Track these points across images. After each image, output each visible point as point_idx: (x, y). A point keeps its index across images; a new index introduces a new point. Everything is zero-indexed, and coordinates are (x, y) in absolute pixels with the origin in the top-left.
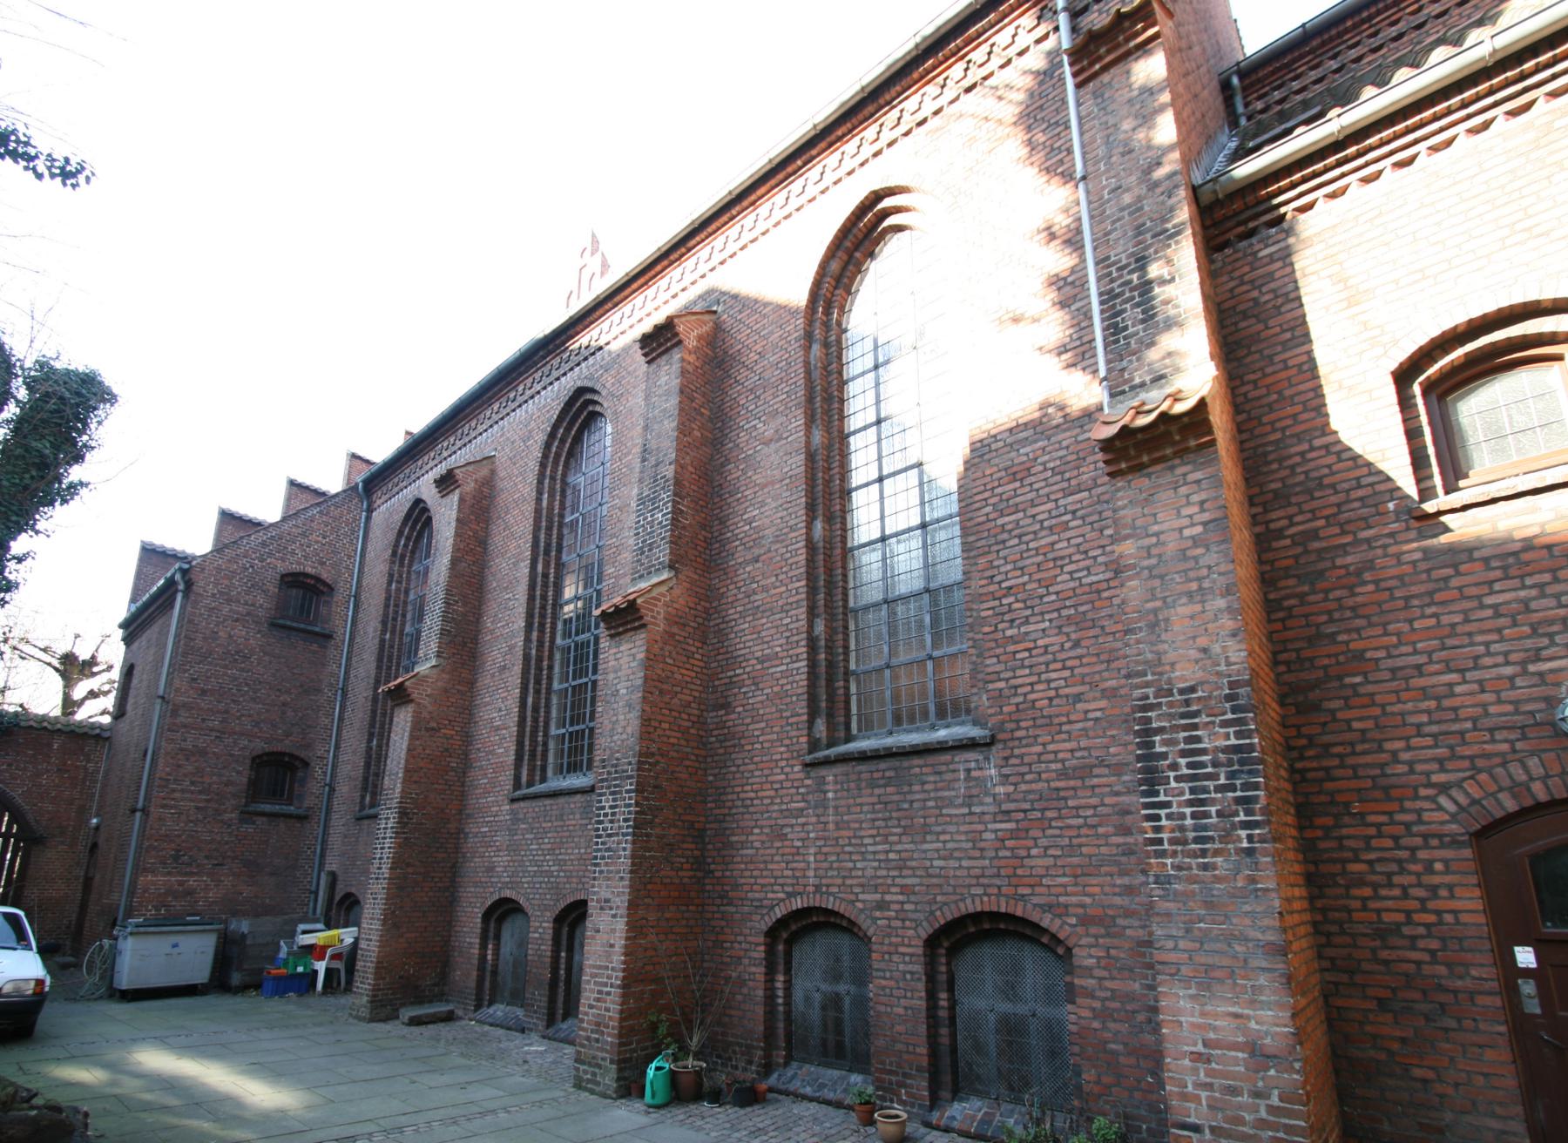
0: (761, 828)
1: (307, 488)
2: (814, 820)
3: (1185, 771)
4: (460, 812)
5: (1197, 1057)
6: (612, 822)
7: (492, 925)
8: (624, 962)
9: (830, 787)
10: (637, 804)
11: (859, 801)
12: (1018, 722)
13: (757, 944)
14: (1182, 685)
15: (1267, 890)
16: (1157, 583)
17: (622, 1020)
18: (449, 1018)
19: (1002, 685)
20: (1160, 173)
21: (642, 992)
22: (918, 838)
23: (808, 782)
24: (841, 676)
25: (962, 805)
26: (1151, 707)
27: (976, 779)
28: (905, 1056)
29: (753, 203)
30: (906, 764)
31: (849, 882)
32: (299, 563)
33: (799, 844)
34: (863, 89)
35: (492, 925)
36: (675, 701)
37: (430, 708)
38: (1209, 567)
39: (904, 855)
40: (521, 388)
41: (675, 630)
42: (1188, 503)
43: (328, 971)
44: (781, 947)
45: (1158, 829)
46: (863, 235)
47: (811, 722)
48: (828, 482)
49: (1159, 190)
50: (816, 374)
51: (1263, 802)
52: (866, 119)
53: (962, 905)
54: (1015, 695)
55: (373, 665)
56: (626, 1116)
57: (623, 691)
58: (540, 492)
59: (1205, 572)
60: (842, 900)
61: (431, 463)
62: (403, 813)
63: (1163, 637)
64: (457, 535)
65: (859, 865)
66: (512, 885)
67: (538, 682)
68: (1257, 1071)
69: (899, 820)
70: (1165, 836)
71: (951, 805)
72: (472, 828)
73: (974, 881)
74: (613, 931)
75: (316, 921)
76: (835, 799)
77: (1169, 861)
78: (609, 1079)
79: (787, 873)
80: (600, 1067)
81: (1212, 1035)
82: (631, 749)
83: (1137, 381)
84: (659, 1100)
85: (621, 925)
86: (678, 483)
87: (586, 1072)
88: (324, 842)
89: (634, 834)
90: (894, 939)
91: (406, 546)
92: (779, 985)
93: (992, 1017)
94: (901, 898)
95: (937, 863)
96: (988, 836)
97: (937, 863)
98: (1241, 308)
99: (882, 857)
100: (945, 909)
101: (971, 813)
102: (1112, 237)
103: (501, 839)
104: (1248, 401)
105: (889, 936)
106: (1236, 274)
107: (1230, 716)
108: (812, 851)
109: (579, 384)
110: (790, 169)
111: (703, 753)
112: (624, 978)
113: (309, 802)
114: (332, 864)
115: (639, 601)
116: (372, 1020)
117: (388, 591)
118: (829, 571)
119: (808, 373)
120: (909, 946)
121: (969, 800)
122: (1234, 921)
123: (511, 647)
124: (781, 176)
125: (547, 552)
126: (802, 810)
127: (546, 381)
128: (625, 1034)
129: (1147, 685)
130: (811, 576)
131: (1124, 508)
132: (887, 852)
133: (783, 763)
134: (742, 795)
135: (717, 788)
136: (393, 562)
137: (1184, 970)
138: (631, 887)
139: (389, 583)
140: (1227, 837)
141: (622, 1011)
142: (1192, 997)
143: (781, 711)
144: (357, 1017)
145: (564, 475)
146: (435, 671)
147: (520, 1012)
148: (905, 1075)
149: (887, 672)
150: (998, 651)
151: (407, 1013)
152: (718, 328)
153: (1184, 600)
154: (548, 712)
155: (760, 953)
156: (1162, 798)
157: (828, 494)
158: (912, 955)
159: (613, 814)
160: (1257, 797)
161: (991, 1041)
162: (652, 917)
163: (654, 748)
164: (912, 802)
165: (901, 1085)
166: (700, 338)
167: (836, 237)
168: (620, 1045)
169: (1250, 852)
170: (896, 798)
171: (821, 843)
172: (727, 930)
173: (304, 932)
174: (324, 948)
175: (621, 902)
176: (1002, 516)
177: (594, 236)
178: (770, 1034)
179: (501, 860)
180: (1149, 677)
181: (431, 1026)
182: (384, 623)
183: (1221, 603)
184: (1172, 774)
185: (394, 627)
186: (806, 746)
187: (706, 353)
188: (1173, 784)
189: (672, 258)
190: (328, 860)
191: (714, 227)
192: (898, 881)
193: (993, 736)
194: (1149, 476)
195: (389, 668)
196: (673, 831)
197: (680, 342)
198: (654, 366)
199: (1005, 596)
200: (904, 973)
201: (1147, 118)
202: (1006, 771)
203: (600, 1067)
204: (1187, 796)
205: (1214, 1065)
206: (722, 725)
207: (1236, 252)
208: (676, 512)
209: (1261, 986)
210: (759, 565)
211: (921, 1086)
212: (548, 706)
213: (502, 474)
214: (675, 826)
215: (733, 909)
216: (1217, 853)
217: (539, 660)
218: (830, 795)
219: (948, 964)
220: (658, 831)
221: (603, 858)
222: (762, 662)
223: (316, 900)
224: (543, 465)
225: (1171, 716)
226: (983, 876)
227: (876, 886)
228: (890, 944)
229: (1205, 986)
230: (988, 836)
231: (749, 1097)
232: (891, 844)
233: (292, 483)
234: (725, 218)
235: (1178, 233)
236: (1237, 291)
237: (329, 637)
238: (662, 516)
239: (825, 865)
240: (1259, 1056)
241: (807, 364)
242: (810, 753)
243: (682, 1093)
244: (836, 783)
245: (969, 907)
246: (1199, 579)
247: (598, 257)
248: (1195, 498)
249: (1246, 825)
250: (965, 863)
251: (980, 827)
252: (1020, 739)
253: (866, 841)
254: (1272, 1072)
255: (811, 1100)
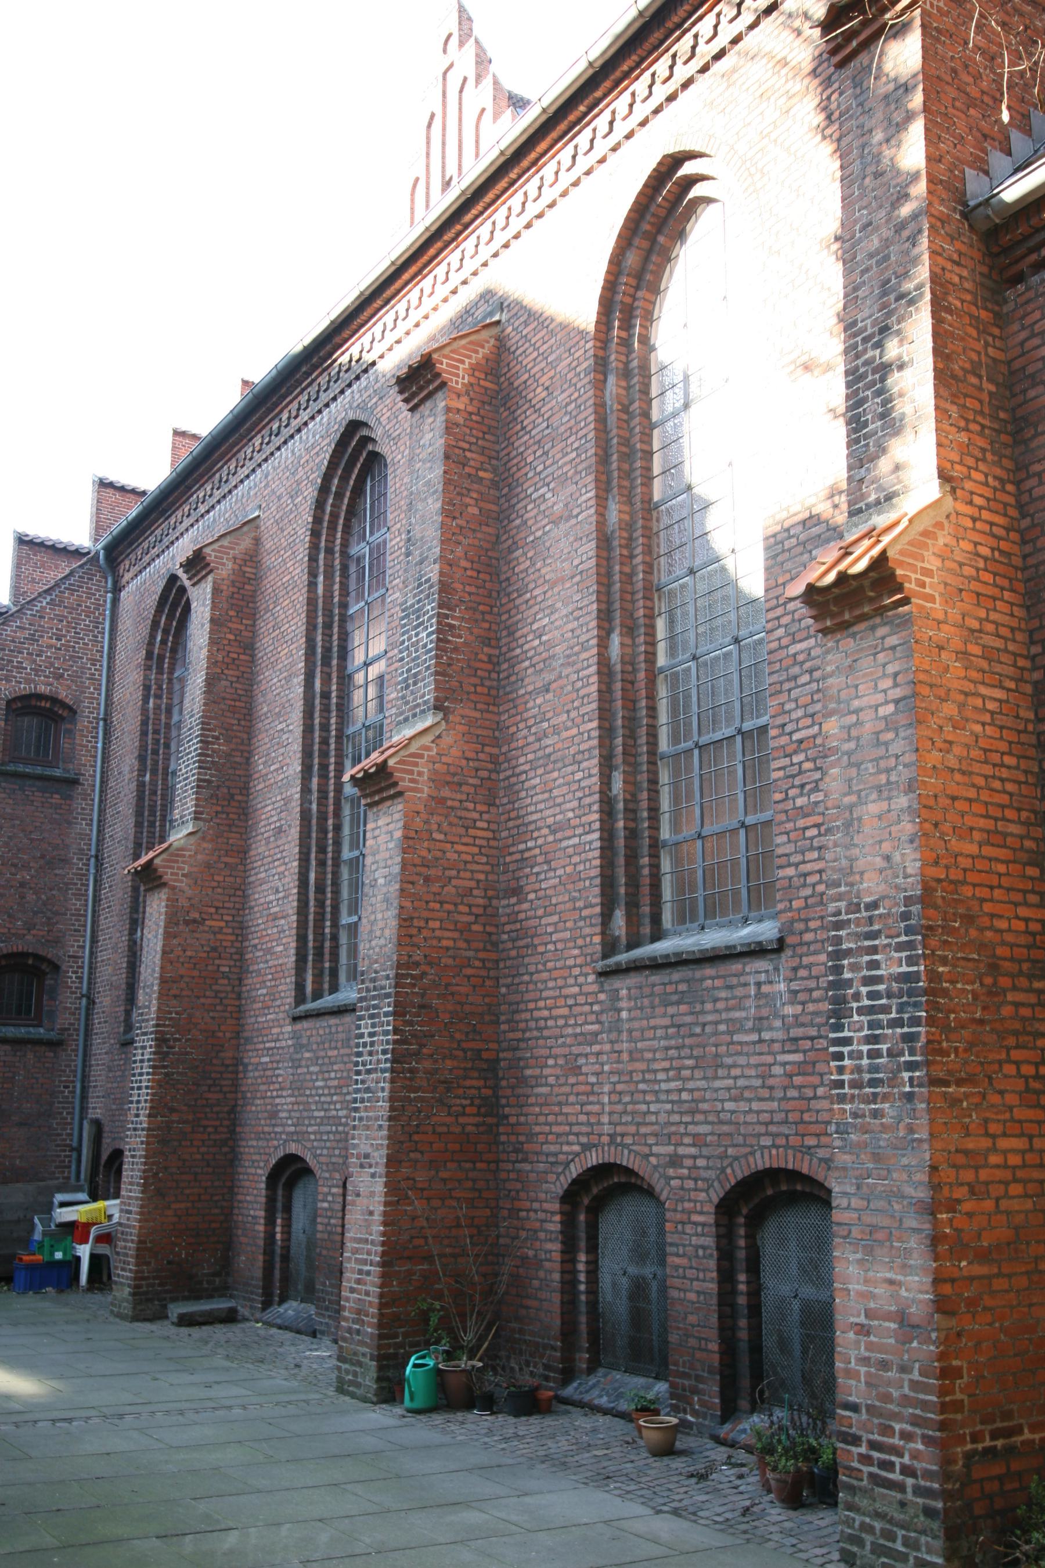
0: (556, 1057)
1: (42, 544)
2: (607, 1047)
3: (867, 1002)
4: (237, 1035)
5: (863, 1330)
6: (370, 1054)
7: (280, 1192)
8: (384, 1234)
9: (623, 1004)
10: (396, 1031)
11: (652, 1022)
12: (807, 921)
13: (553, 1213)
14: (868, 900)
15: (920, 1141)
16: (853, 772)
17: (382, 1306)
18: (230, 1318)
19: (790, 871)
20: (906, 210)
21: (410, 1273)
22: (710, 1073)
23: (602, 997)
24: (645, 850)
25: (752, 1030)
26: (839, 925)
27: (766, 996)
28: (698, 1355)
29: (534, 163)
30: (698, 974)
31: (643, 1130)
32: (28, 681)
33: (593, 1079)
34: (641, 14)
35: (280, 1192)
36: (449, 889)
37: (189, 892)
38: (897, 757)
39: (696, 1094)
40: (285, 416)
41: (446, 792)
42: (884, 675)
43: (93, 1257)
44: (582, 1217)
45: (841, 1070)
46: (664, 208)
47: (607, 916)
48: (628, 578)
49: (905, 234)
50: (612, 420)
51: (923, 1039)
52: (656, 48)
53: (751, 1159)
54: (804, 885)
55: (131, 821)
56: (381, 1416)
57: (381, 881)
58: (313, 574)
59: (892, 762)
60: (637, 1153)
61: (187, 522)
62: (161, 1040)
63: (856, 841)
64: (212, 642)
65: (653, 1108)
66: (299, 1136)
67: (322, 849)
68: (904, 1343)
69: (691, 1048)
70: (846, 1077)
71: (741, 1030)
72: (252, 1058)
73: (762, 1129)
74: (372, 1194)
75: (78, 1189)
76: (630, 1020)
77: (848, 1107)
78: (369, 1380)
79: (583, 1118)
80: (360, 1364)
81: (872, 1305)
82: (389, 958)
83: (872, 498)
84: (417, 1404)
85: (379, 1187)
86: (444, 588)
87: (347, 1372)
88: (85, 1077)
89: (392, 1070)
90: (687, 1205)
91: (164, 642)
92: (581, 1267)
93: (796, 1305)
94: (693, 1151)
95: (729, 1106)
96: (777, 1070)
97: (729, 1106)
98: (1030, 370)
99: (674, 1097)
100: (736, 1164)
101: (761, 1041)
102: (860, 293)
103: (284, 1072)
104: (1033, 500)
105: (682, 1200)
106: (1027, 321)
107: (903, 938)
108: (606, 1089)
109: (351, 416)
110: (572, 118)
111: (493, 956)
112: (384, 1254)
113: (63, 1020)
114: (97, 1110)
115: (391, 763)
116: (135, 1318)
117: (144, 711)
118: (631, 704)
119: (601, 420)
120: (701, 1213)
121: (760, 1023)
122: (895, 1175)
123: (287, 801)
124: (563, 126)
125: (326, 661)
126: (596, 1034)
127: (314, 407)
128: (387, 1324)
129: (839, 898)
130: (605, 714)
131: (831, 675)
132: (680, 1091)
133: (576, 971)
134: (536, 1014)
135: (510, 1004)
136: (148, 668)
137: (855, 1232)
138: (389, 1138)
139: (146, 700)
140: (893, 1080)
141: (381, 1296)
142: (860, 1262)
143: (574, 900)
144: (119, 1316)
145: (345, 545)
146: (192, 839)
147: (312, 1309)
148: (699, 1379)
149: (699, 843)
150: (789, 826)
151: (176, 1310)
152: (501, 347)
153: (874, 796)
154: (336, 892)
155: (555, 1225)
156: (846, 1034)
157: (628, 593)
158: (704, 1225)
159: (372, 1044)
160: (919, 1033)
161: (796, 1335)
162: (421, 1176)
163: (418, 955)
164: (704, 1025)
165: (695, 1391)
166: (474, 369)
167: (628, 219)
168: (381, 1337)
169: (910, 1097)
170: (688, 1019)
171: (614, 1078)
172: (522, 1195)
173: (63, 1205)
174: (87, 1226)
175: (380, 1157)
176: (794, 642)
177: (462, 10)
178: (568, 1331)
179: (285, 1101)
180: (843, 889)
181: (204, 1328)
182: (142, 759)
183: (903, 801)
184: (855, 1005)
185: (155, 763)
186: (599, 948)
187: (483, 383)
188: (856, 1018)
189: (446, 237)
190: (92, 1102)
191: (490, 196)
192: (691, 1128)
193: (781, 940)
194: (853, 635)
195: (152, 824)
196: (449, 1064)
197: (444, 384)
198: (417, 415)
199: (795, 752)
200: (697, 1247)
201: (897, 128)
202: (795, 986)
203: (360, 1364)
204: (866, 1032)
205: (872, 1338)
206: (514, 918)
207: (1028, 289)
208: (444, 630)
209: (912, 1249)
210: (549, 696)
211: (712, 1390)
212: (336, 884)
213: (268, 545)
214: (453, 1057)
215: (527, 1167)
216: (885, 1097)
217: (323, 817)
218: (624, 1014)
219: (751, 1237)
220: (427, 1064)
221: (362, 1101)
222: (554, 832)
223: (79, 1161)
224: (315, 534)
225: (858, 936)
226: (771, 1123)
227: (669, 1135)
228: (683, 1211)
229: (869, 1250)
230: (777, 1070)
231: (528, 1404)
232: (685, 1080)
233: (24, 542)
234: (503, 184)
235: (912, 302)
236: (1029, 345)
237: (74, 782)
238: (426, 637)
239: (619, 1108)
240: (901, 1317)
241: (600, 407)
242: (605, 957)
243: (452, 1397)
244: (630, 998)
245: (761, 1162)
246: (888, 771)
247: (470, 47)
248: (891, 669)
249: (911, 1066)
250: (755, 1106)
251: (769, 1059)
252: (808, 944)
253: (661, 1076)
254: (915, 1344)
255: (605, 1412)
